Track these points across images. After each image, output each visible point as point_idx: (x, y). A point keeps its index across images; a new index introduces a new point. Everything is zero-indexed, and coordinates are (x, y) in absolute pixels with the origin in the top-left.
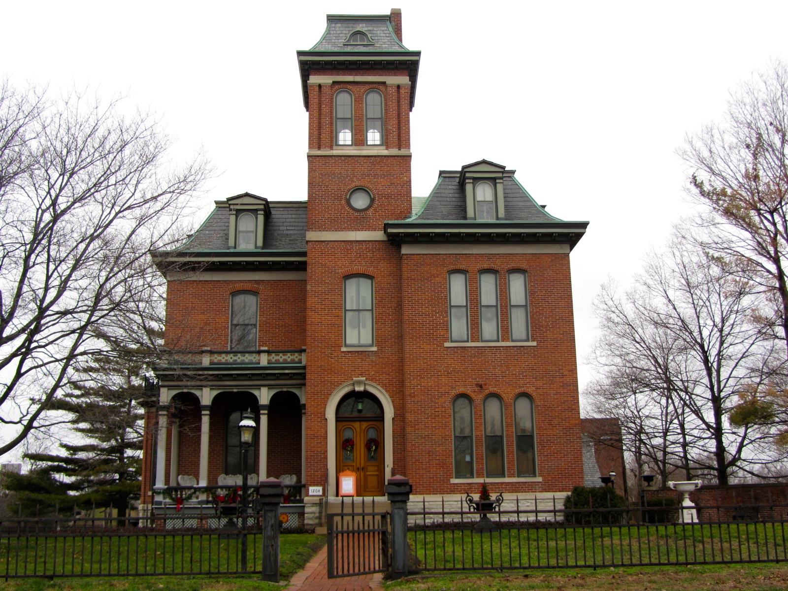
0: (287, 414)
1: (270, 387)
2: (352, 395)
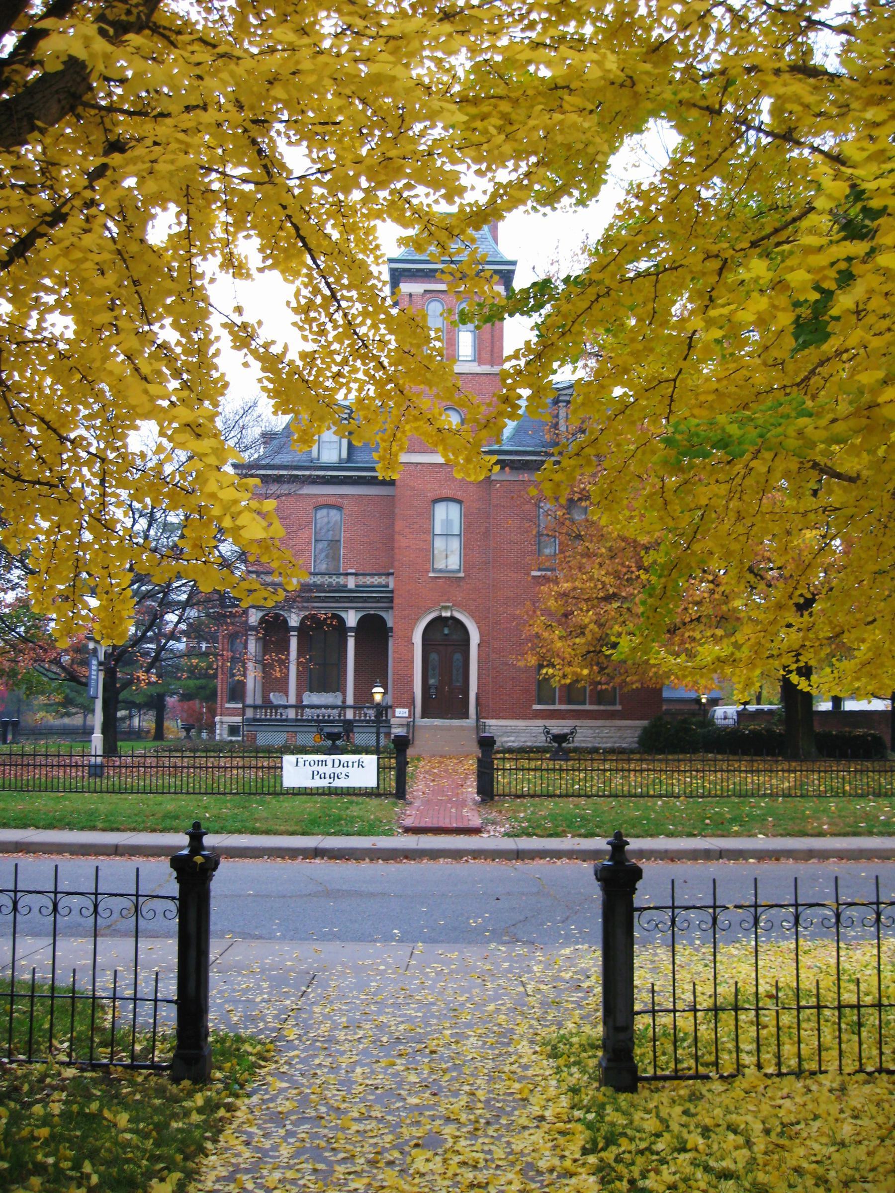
0: (374, 633)
1: (357, 609)
2: (439, 620)
